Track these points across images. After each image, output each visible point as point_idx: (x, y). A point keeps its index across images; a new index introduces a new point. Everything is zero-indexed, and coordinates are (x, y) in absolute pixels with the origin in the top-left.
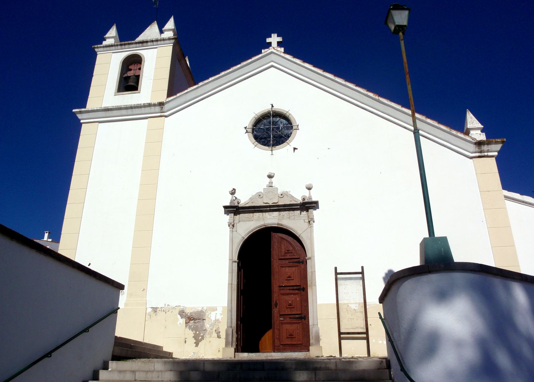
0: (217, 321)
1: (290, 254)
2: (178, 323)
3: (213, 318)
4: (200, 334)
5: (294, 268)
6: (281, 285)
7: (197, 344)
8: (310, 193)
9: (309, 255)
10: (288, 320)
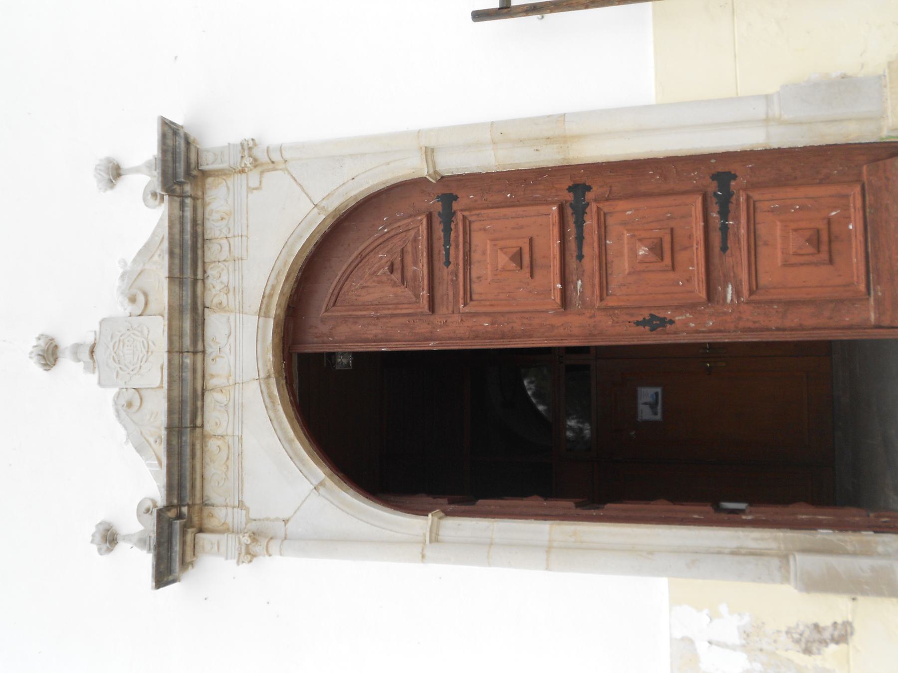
1: (409, 259)
5: (478, 239)
6: (556, 297)
8: (136, 170)
9: (412, 166)
10: (737, 260)
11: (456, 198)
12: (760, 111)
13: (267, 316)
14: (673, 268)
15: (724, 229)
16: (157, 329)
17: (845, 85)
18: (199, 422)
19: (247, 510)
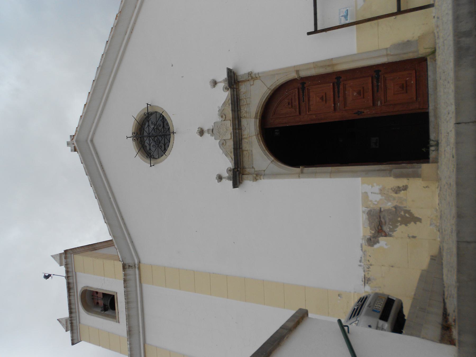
0: (382, 191)
2: (386, 247)
3: (378, 197)
4: (402, 217)
7: (417, 220)
8: (220, 82)
9: (293, 75)
11: (305, 83)
12: (385, 53)
13: (257, 119)
14: (364, 98)
15: (378, 86)
16: (229, 124)
17: (408, 43)
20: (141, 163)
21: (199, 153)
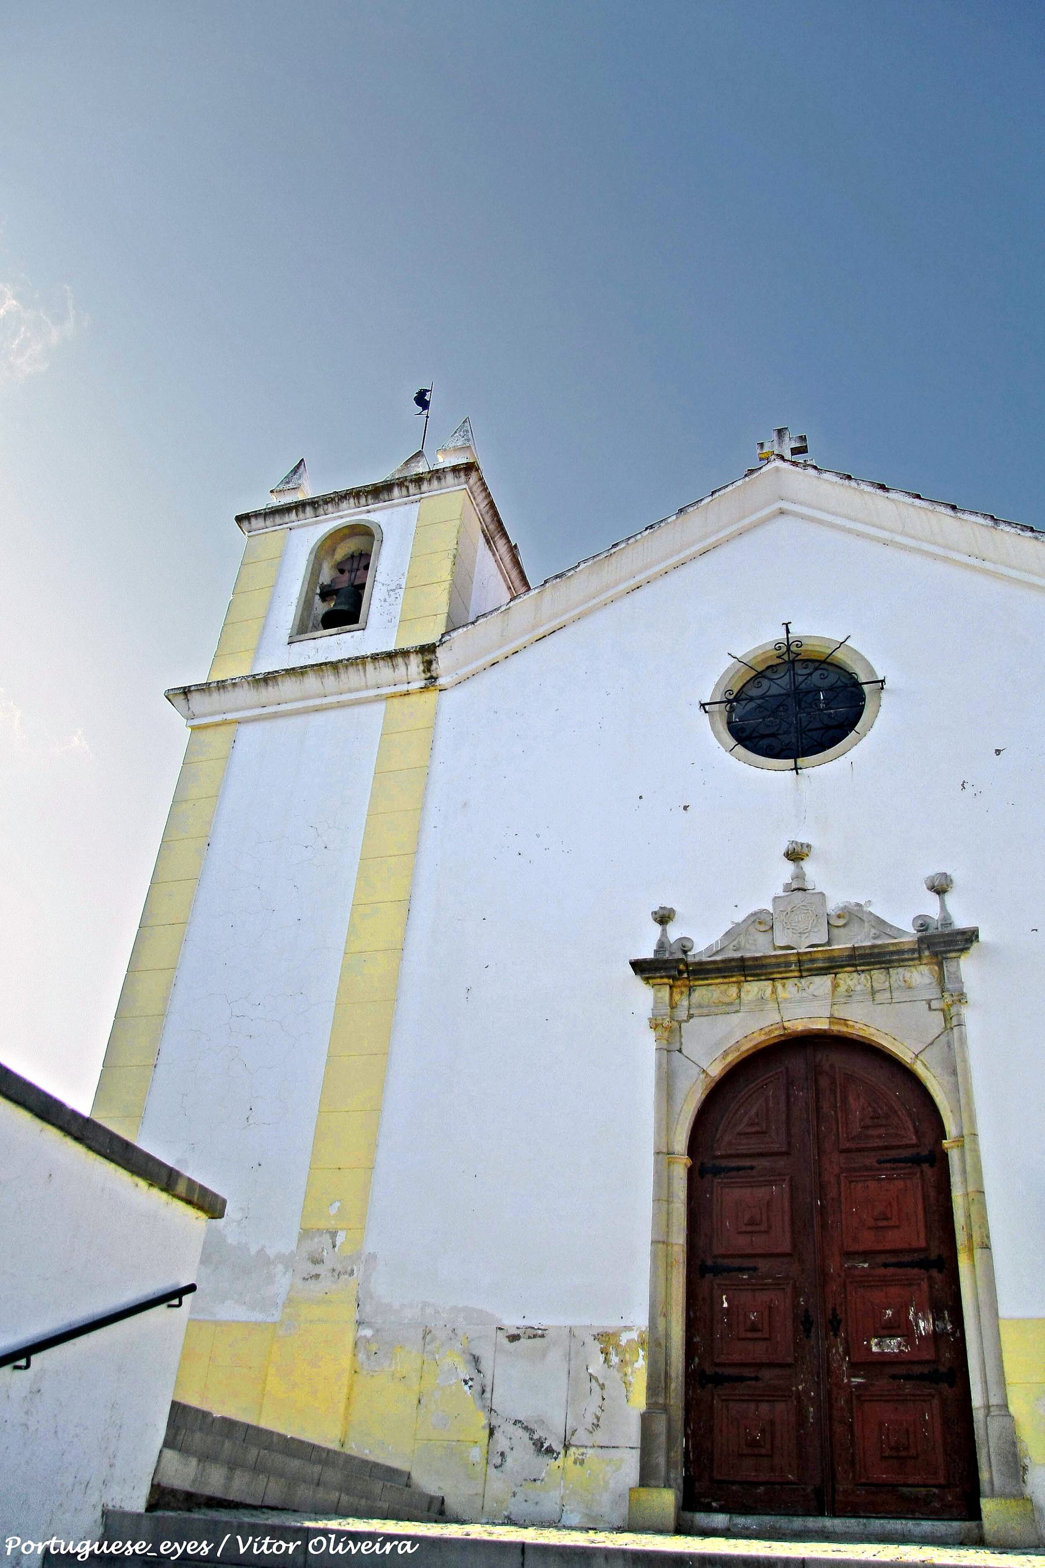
11: (932, 1166)
18: (749, 979)
19: (687, 1021)
20: (712, 675)
21: (737, 850)
